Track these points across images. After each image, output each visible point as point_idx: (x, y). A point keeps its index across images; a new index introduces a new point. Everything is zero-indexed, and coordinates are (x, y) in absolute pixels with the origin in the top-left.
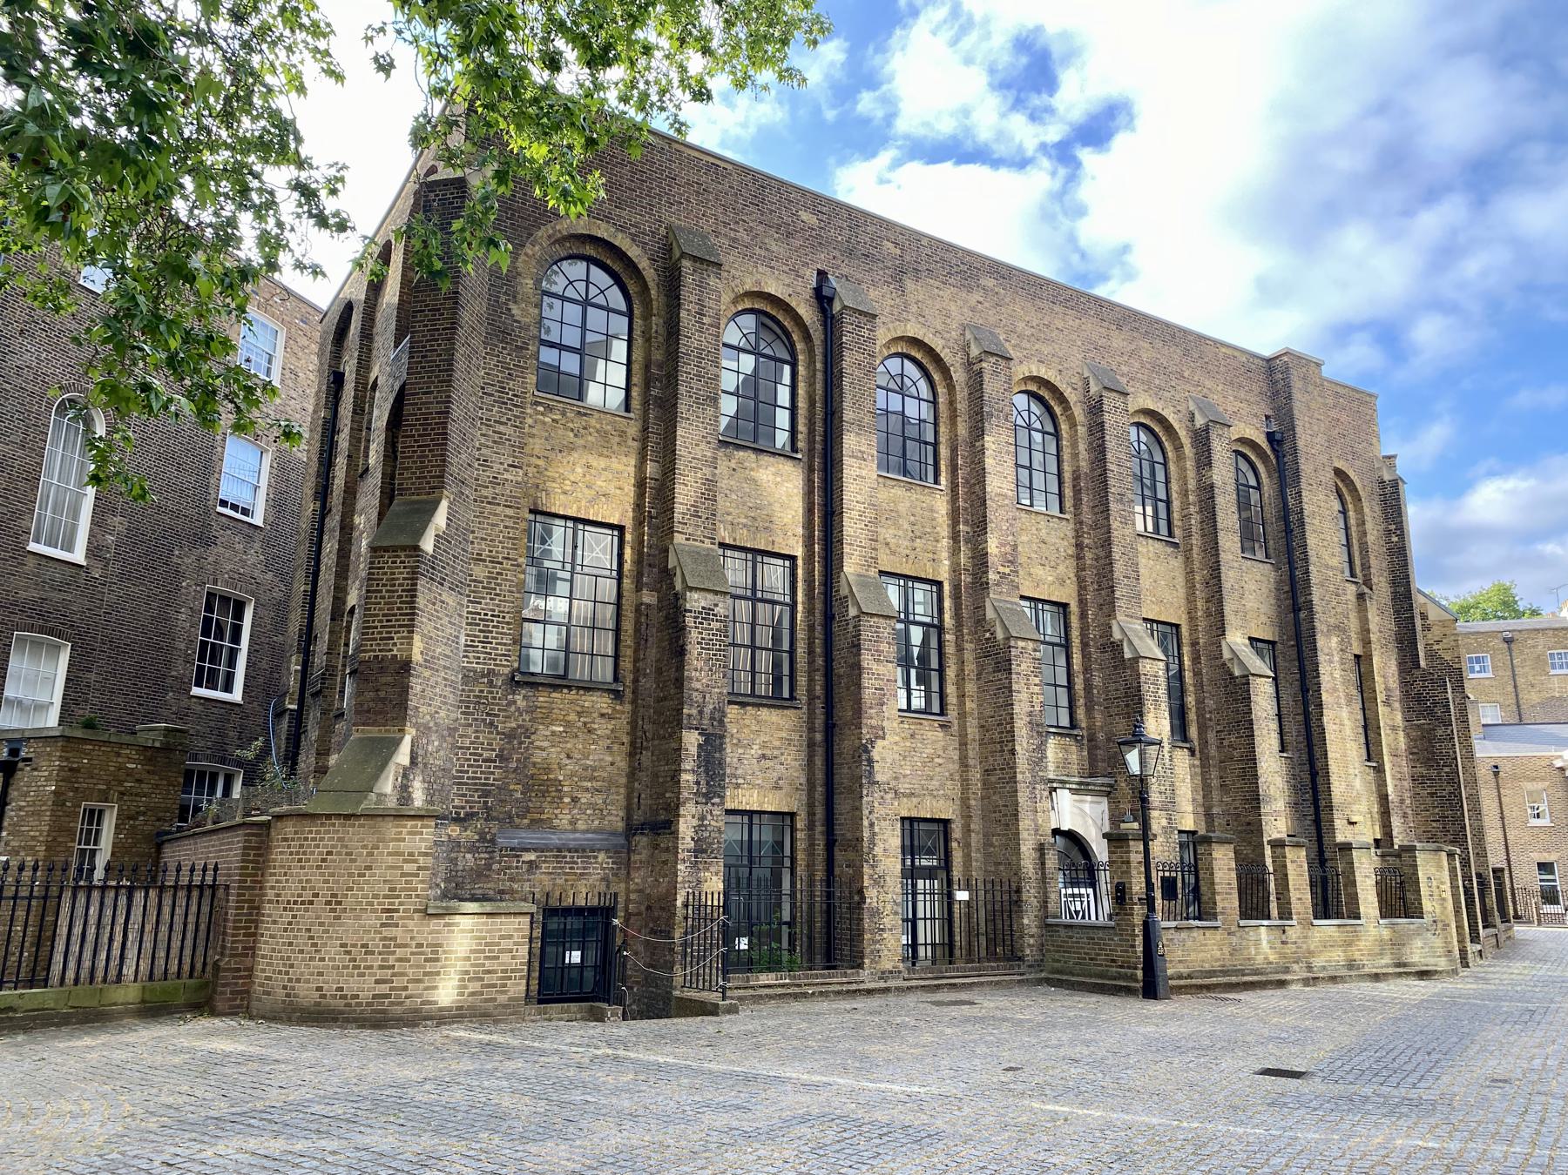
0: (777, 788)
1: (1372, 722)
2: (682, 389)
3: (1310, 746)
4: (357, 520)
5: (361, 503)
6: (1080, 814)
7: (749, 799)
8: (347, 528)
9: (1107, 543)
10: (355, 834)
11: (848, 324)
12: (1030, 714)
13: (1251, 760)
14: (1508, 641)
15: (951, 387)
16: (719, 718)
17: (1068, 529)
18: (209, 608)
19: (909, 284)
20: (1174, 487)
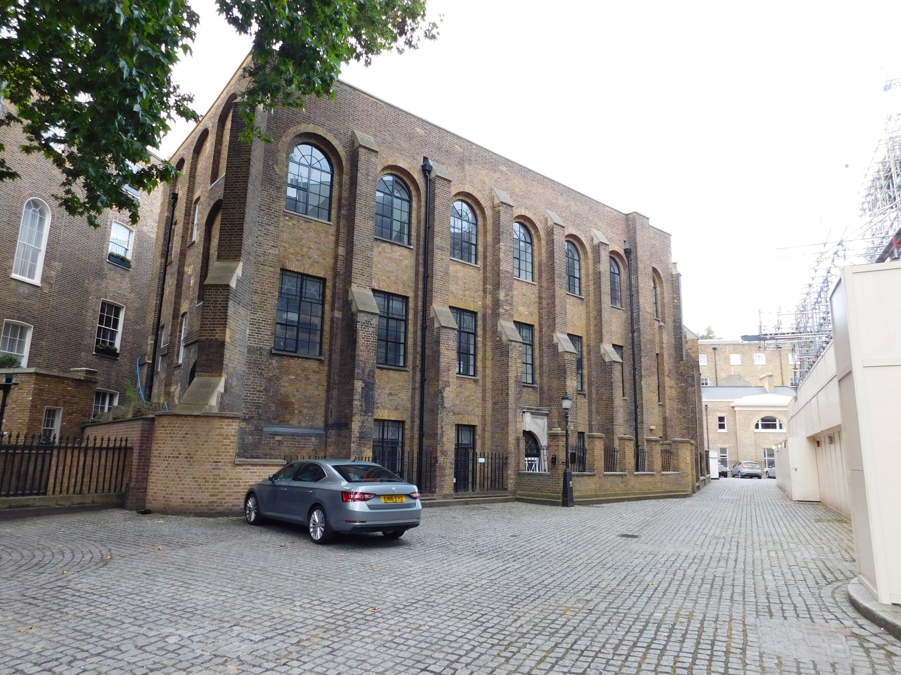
0: (396, 409)
1: (661, 384)
2: (357, 212)
3: (635, 395)
4: (186, 269)
5: (189, 260)
6: (538, 426)
7: (383, 414)
8: (181, 274)
9: (553, 297)
10: (201, 425)
11: (439, 184)
12: (516, 377)
13: (611, 400)
14: (715, 349)
15: (484, 217)
16: (372, 375)
17: (536, 290)
18: (102, 310)
19: (467, 167)
20: (583, 272)
